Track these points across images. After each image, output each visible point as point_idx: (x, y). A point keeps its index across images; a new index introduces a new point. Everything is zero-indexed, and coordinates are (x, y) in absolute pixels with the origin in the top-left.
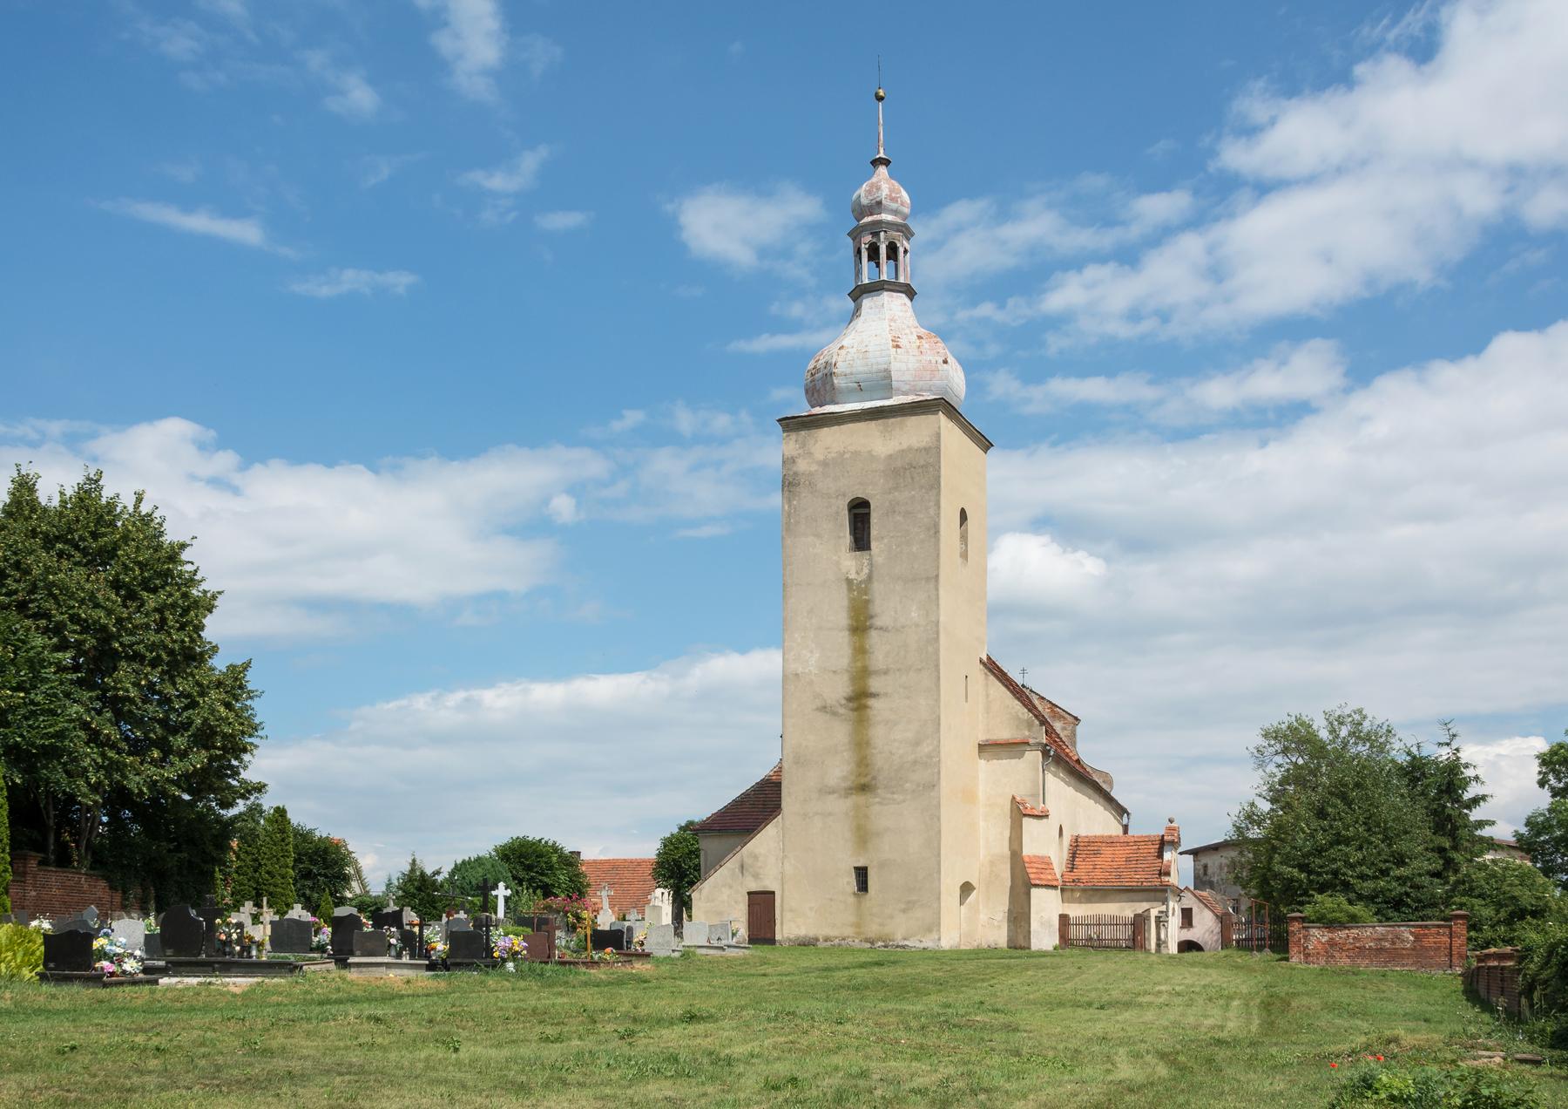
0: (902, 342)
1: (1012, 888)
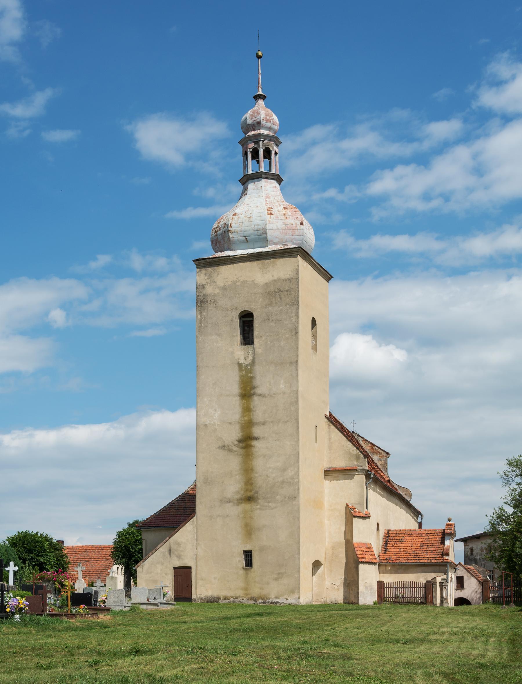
0: (274, 211)
1: (347, 564)
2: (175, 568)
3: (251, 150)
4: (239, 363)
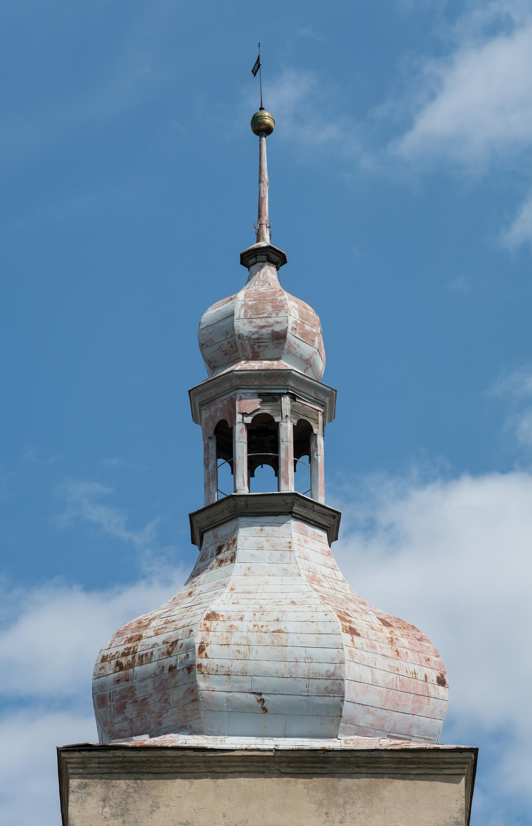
0: (359, 624)
3: (249, 420)
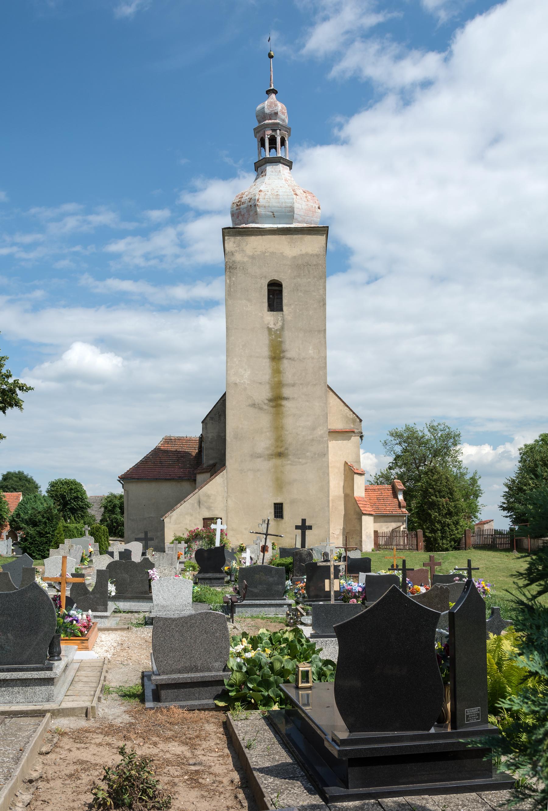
1: (345, 515)
2: (204, 519)
3: (269, 136)
4: (268, 328)
